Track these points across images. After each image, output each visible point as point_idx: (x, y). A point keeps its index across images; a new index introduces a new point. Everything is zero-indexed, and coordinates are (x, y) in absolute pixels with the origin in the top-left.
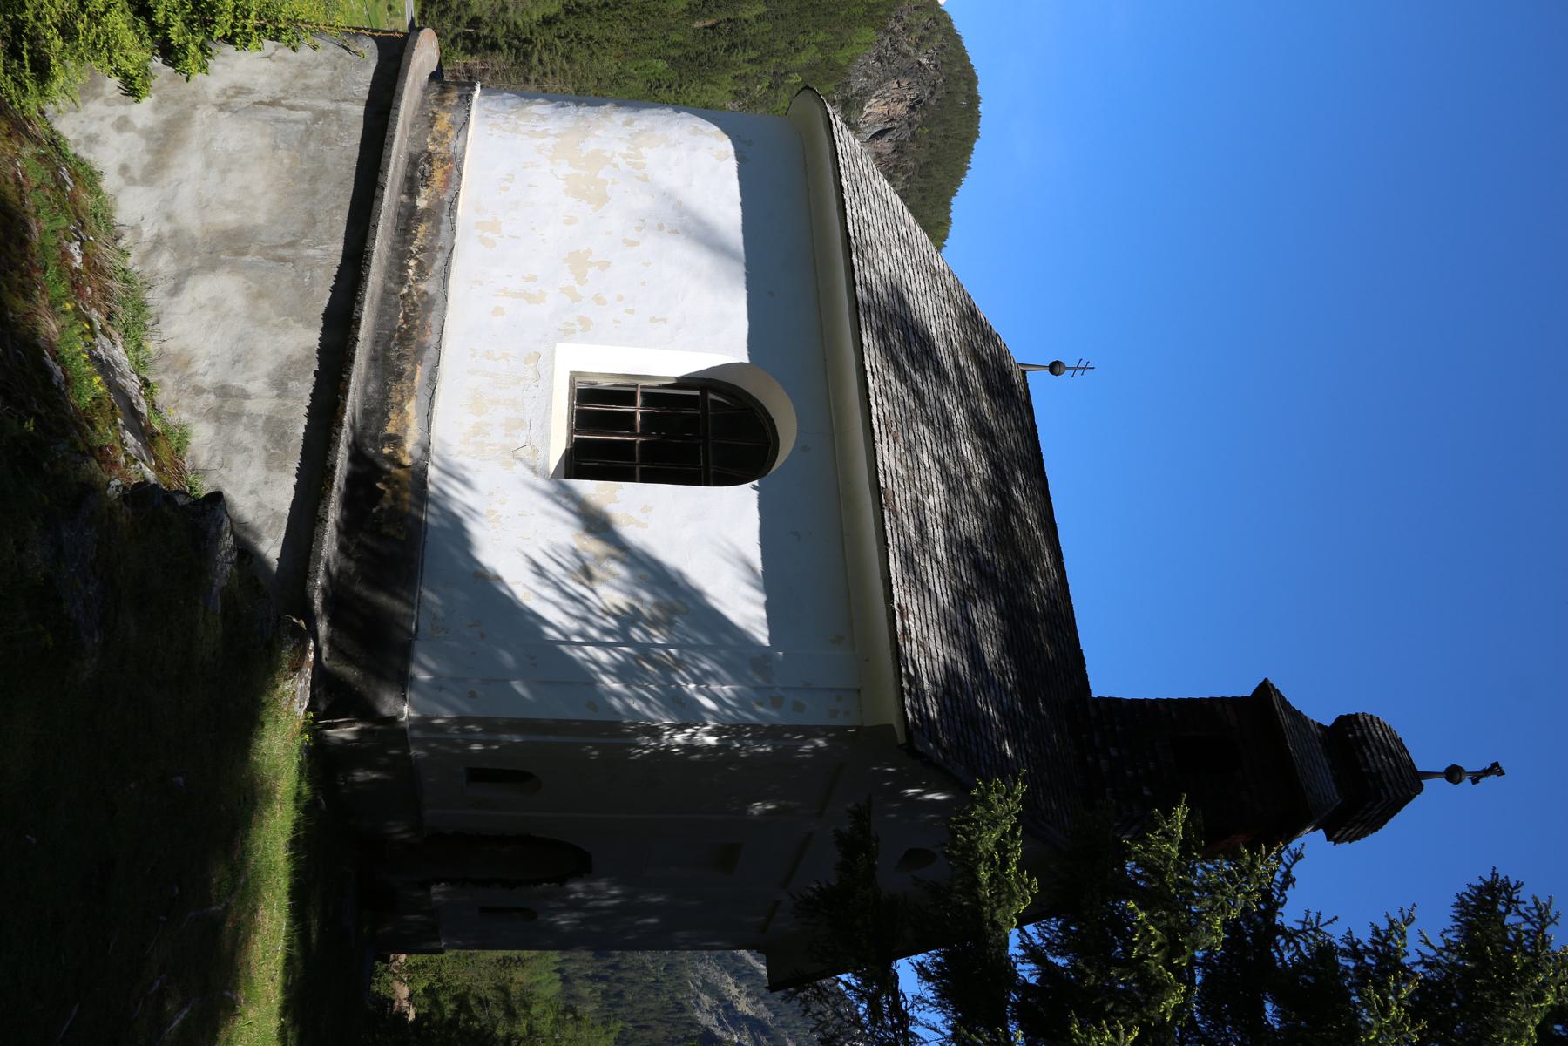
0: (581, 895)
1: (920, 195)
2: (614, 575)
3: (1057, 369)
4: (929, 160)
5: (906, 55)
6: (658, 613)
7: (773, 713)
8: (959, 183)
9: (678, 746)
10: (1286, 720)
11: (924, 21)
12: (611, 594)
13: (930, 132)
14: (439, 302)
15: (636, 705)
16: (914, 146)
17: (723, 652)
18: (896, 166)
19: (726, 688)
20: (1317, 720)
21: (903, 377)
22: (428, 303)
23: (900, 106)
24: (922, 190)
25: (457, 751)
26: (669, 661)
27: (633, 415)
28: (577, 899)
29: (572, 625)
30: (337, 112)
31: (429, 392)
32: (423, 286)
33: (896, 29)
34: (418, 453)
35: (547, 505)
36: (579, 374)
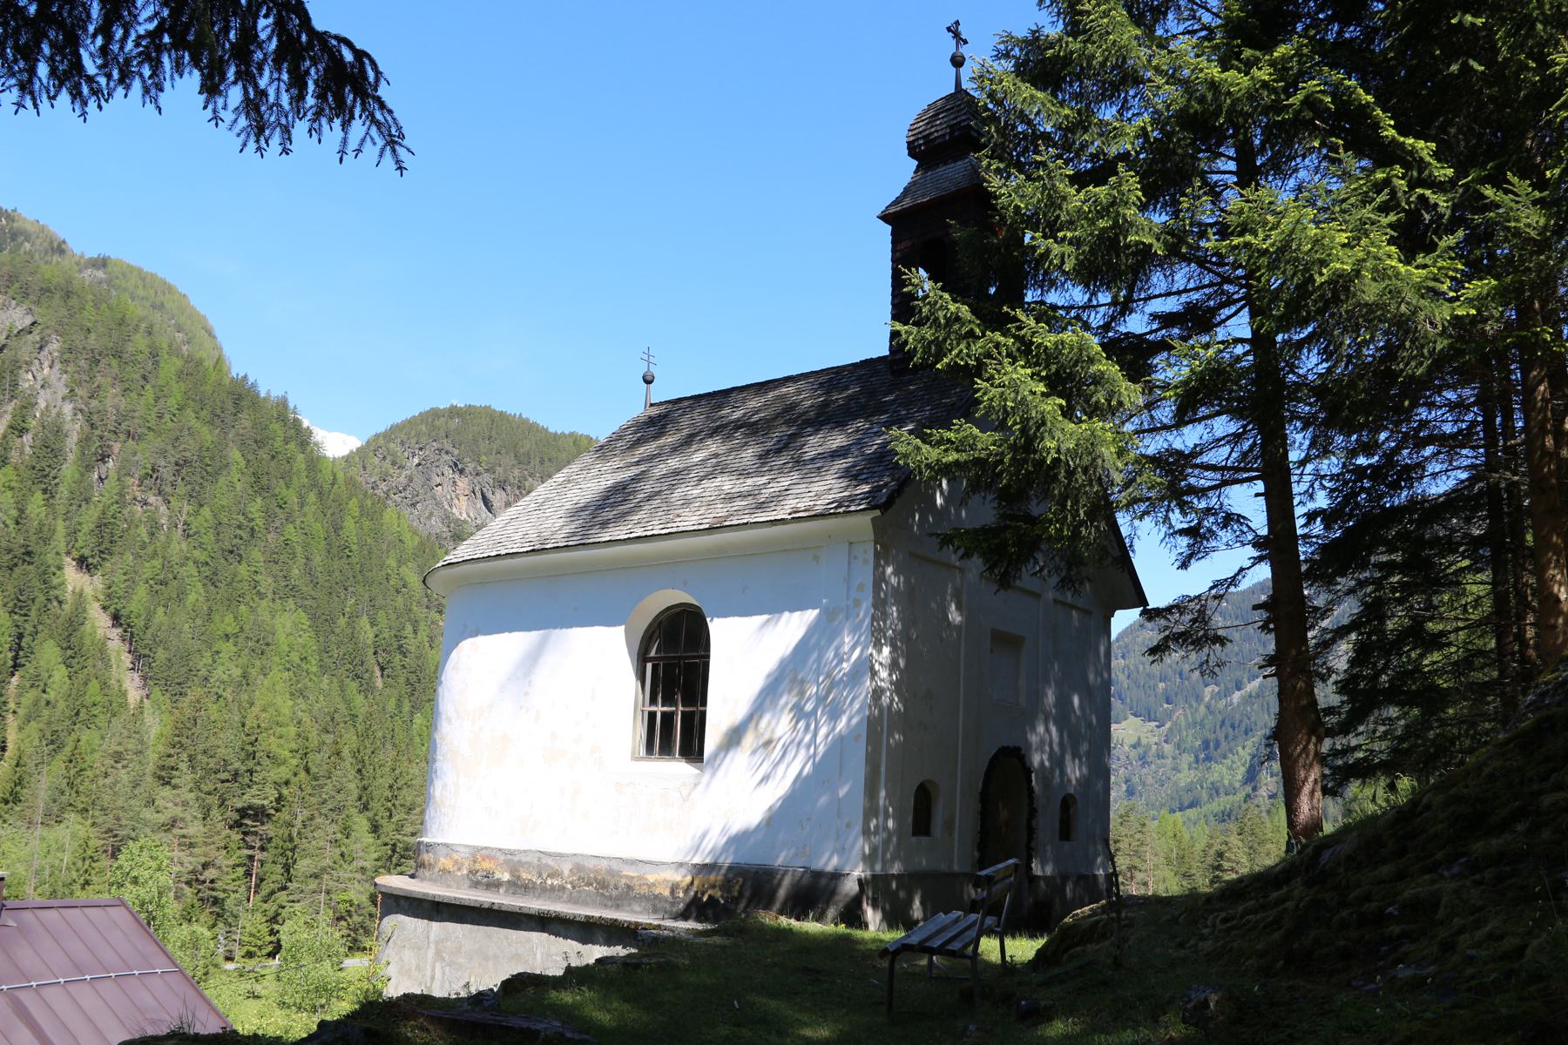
0: (1045, 757)
1: (547, 463)
2: (769, 723)
3: (649, 378)
4: (512, 455)
5: (411, 479)
6: (795, 692)
7: (864, 606)
8: (535, 425)
9: (890, 675)
10: (907, 203)
11: (376, 461)
12: (781, 725)
13: (486, 454)
14: (577, 860)
15: (856, 706)
16: (499, 470)
17: (823, 643)
18: (519, 487)
19: (847, 640)
20: (912, 175)
21: (638, 507)
22: (578, 868)
23: (459, 483)
24: (542, 462)
25: (895, 839)
26: (827, 682)
27: (664, 714)
28: (1050, 758)
29: (803, 752)
30: (437, 943)
31: (641, 865)
32: (566, 873)
33: (385, 489)
34: (683, 871)
35: (721, 773)
36: (633, 753)
